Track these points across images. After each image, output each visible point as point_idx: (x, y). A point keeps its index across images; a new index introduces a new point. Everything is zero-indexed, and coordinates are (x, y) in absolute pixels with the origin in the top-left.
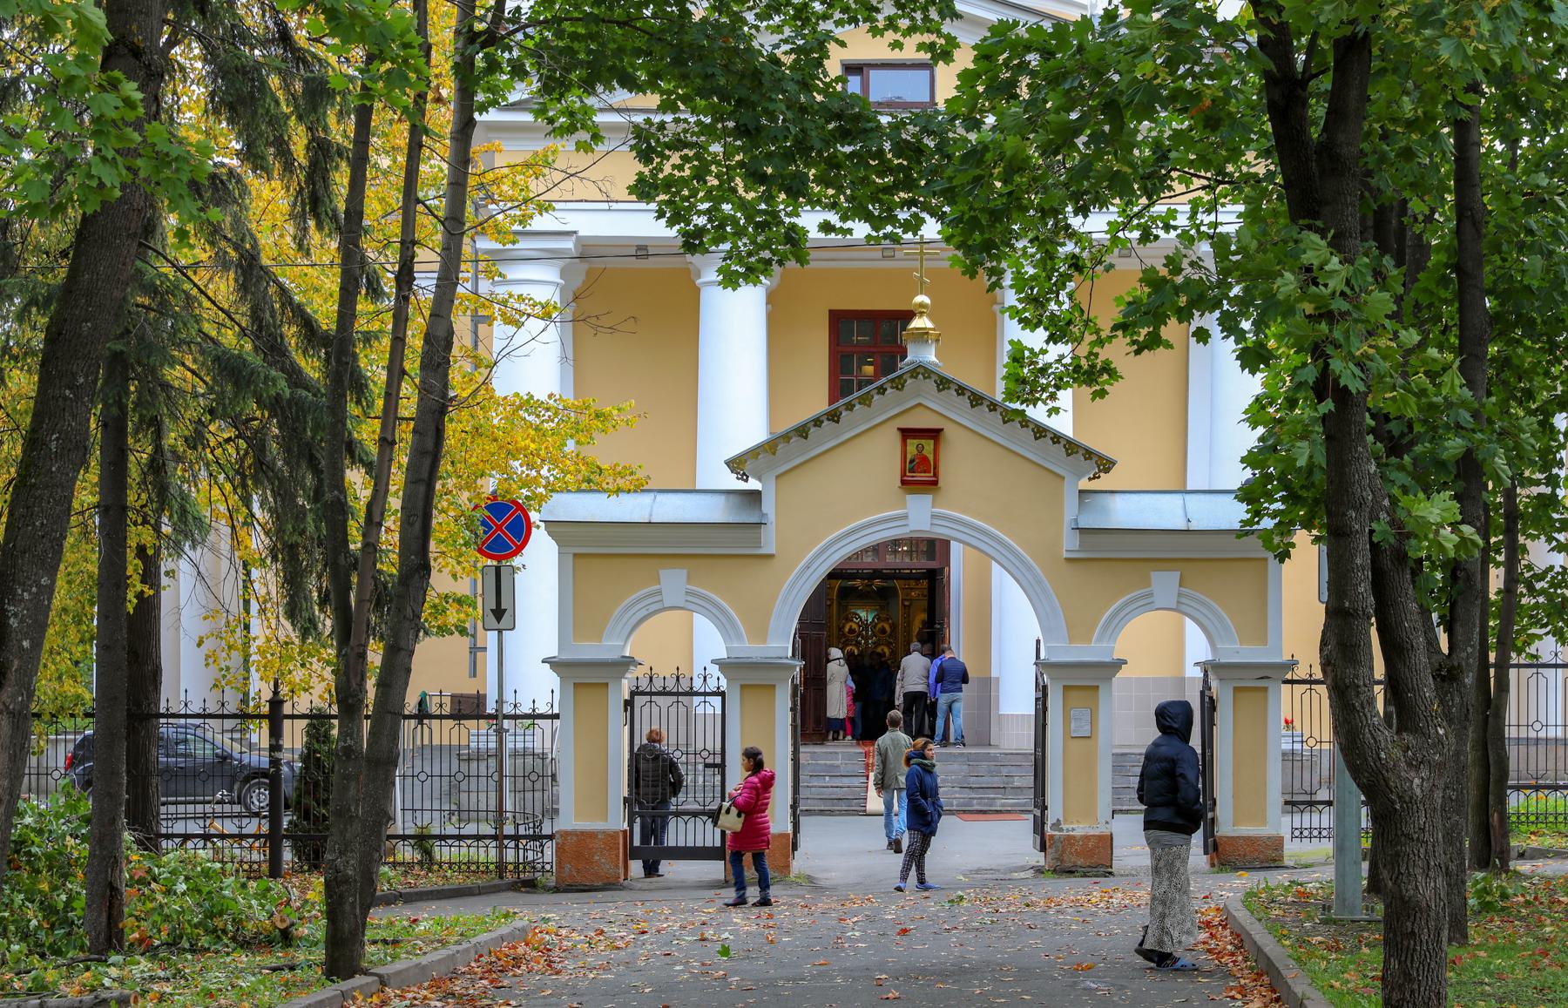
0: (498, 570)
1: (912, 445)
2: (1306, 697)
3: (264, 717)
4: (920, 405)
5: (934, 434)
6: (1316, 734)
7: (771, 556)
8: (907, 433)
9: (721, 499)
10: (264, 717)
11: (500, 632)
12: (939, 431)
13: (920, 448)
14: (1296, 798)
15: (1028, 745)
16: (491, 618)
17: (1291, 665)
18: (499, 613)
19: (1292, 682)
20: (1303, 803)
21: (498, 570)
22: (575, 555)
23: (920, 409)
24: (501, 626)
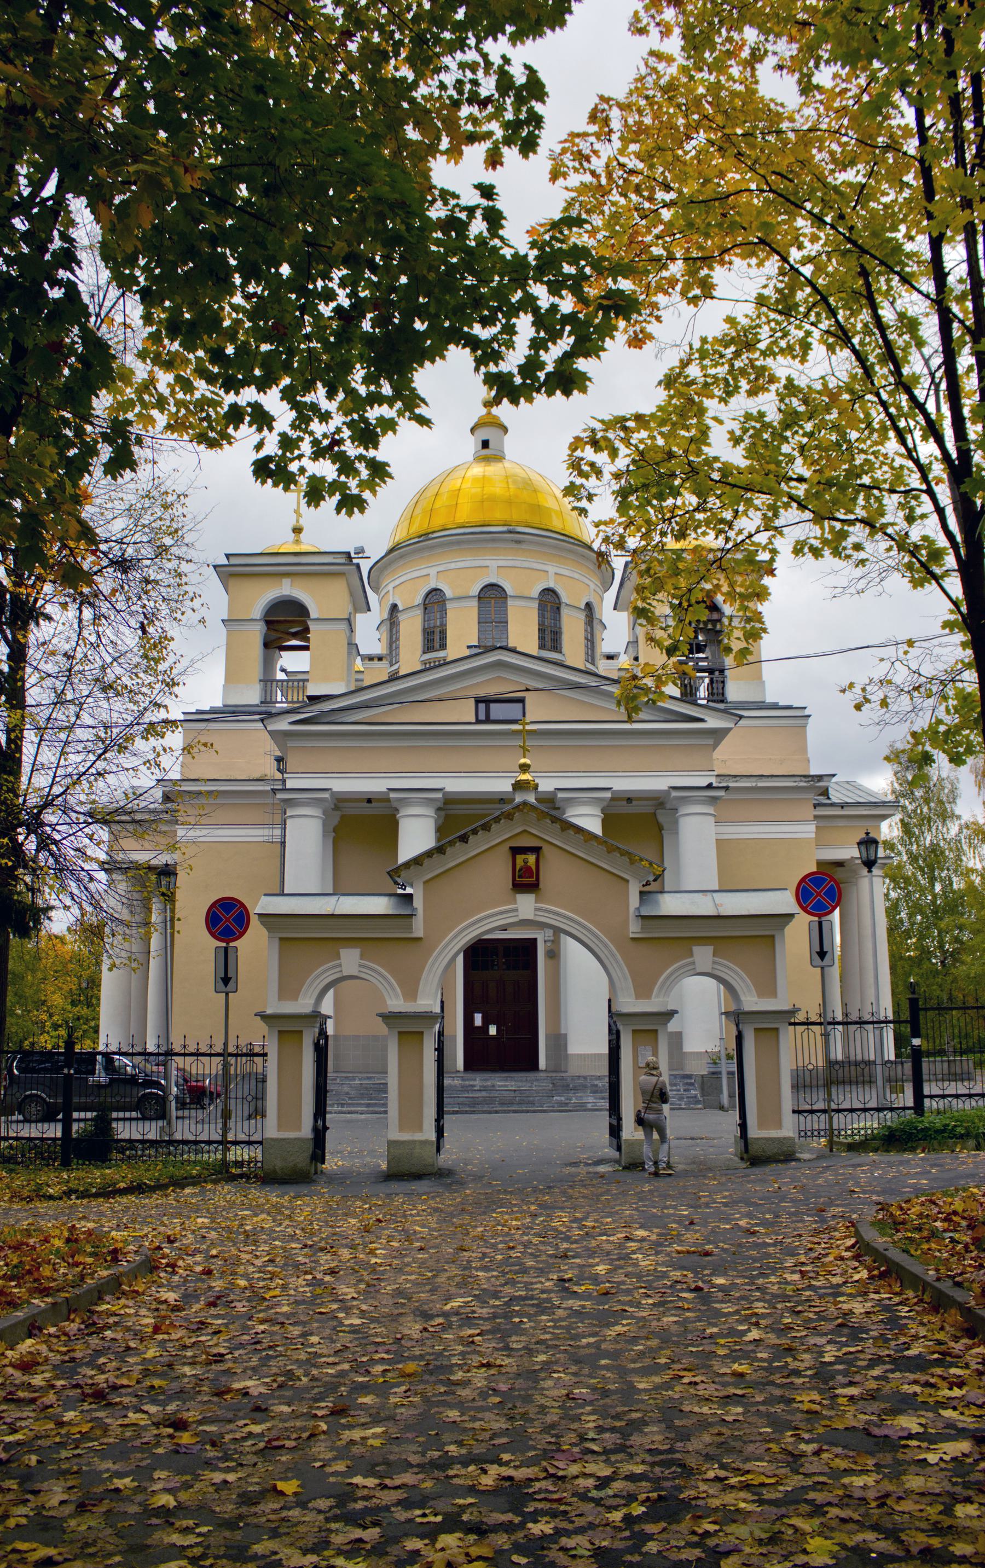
1: (520, 859)
5: (536, 850)
7: (419, 939)
8: (516, 851)
16: (221, 984)
18: (226, 980)
19: (795, 1024)
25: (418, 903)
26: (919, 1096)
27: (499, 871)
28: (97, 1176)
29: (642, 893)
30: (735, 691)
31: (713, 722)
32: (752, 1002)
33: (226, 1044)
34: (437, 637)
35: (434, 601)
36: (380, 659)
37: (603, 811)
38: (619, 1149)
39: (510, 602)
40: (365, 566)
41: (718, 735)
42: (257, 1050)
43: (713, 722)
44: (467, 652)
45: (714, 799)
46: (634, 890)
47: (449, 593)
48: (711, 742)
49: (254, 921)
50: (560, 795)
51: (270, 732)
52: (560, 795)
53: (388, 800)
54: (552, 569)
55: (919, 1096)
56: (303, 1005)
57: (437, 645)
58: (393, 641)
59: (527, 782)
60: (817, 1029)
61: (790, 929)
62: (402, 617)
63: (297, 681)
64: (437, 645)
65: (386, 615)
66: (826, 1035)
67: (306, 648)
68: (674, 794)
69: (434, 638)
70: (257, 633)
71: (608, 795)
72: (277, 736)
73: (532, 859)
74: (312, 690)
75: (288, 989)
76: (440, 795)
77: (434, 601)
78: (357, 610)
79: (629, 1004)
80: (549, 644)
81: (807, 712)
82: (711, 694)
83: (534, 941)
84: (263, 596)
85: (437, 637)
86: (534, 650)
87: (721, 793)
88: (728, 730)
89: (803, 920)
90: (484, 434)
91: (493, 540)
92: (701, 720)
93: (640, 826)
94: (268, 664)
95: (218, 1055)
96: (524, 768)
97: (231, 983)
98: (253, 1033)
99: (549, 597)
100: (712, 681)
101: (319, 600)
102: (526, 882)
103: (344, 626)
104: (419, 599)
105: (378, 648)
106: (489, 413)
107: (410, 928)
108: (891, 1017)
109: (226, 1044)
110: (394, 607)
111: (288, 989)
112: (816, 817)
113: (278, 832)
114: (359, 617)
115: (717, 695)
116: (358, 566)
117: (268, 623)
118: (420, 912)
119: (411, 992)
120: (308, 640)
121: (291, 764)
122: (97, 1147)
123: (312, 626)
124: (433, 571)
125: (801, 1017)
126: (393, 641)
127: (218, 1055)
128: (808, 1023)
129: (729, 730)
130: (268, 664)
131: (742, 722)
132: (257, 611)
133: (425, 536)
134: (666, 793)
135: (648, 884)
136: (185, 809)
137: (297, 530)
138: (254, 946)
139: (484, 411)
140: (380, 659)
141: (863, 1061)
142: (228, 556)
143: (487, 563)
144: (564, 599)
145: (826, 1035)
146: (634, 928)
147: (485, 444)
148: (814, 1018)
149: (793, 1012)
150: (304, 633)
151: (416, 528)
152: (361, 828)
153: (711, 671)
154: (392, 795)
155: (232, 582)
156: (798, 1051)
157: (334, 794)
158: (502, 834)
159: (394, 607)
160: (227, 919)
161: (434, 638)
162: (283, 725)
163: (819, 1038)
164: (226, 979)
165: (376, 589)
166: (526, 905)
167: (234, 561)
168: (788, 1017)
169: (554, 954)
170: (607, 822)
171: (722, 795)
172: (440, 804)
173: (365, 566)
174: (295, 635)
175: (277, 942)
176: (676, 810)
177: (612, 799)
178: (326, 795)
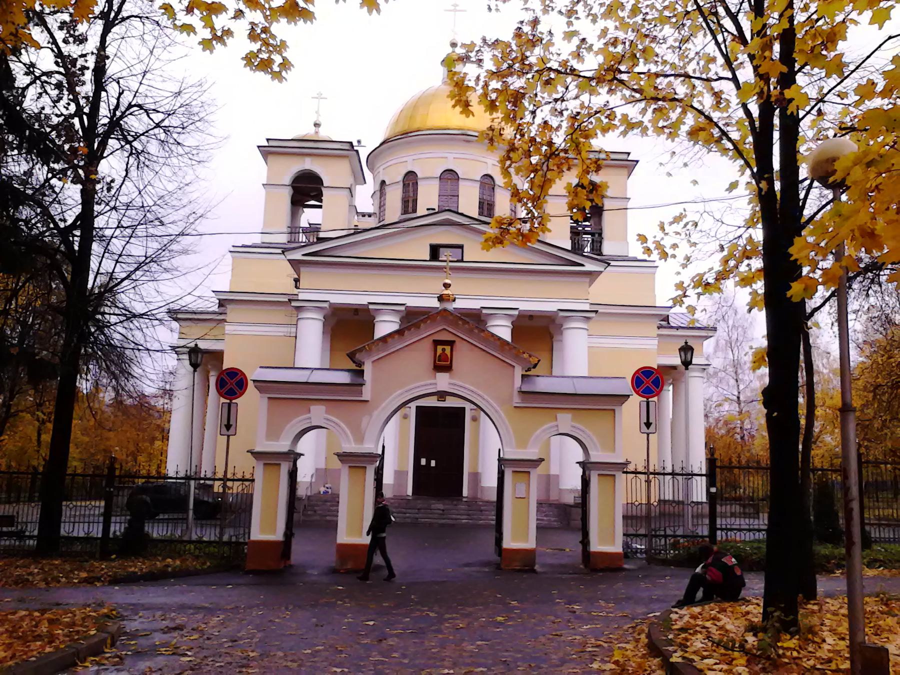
0: (229, 405)
1: (440, 348)
2: (634, 480)
3: (719, 529)
4: (444, 329)
5: (451, 343)
6: (639, 499)
7: (367, 401)
8: (436, 343)
9: (347, 373)
10: (719, 529)
11: (228, 436)
12: (454, 342)
13: (444, 350)
14: (742, 527)
15: (494, 498)
16: (224, 429)
17: (627, 463)
18: (228, 426)
19: (627, 473)
20: (875, 524)
21: (229, 405)
22: (514, 472)
23: (445, 332)
24: (230, 433)
25: (368, 376)
26: (713, 528)
27: (423, 356)
28: (138, 566)
29: (523, 376)
30: (608, 248)
31: (590, 266)
32: (597, 456)
33: (226, 472)
34: (411, 205)
35: (410, 180)
36: (370, 216)
37: (512, 323)
38: (500, 555)
39: (461, 183)
40: (364, 154)
41: (592, 276)
42: (248, 476)
43: (590, 266)
44: (427, 213)
45: (588, 318)
46: (519, 372)
47: (419, 175)
48: (588, 280)
49: (250, 384)
50: (484, 311)
51: (289, 260)
52: (484, 311)
53: (368, 310)
55: (713, 528)
56: (283, 445)
57: (410, 210)
58: (382, 206)
59: (448, 295)
60: (643, 477)
61: (627, 405)
62: (388, 190)
63: (314, 229)
64: (410, 210)
65: (378, 187)
66: (648, 482)
67: (320, 207)
68: (562, 314)
69: (409, 204)
70: (286, 195)
71: (516, 313)
72: (295, 264)
74: (322, 235)
75: (273, 432)
76: (403, 308)
77: (410, 180)
78: (357, 182)
79: (509, 454)
80: (485, 213)
82: (592, 249)
84: (291, 168)
85: (411, 205)
86: (476, 216)
87: (593, 315)
88: (601, 272)
89: (635, 400)
91: (452, 140)
92: (583, 265)
93: (537, 333)
94: (294, 216)
95: (220, 479)
96: (447, 286)
97: (232, 429)
98: (242, 464)
99: (488, 181)
100: (593, 240)
101: (331, 174)
102: (443, 365)
103: (347, 192)
104: (400, 178)
105: (370, 209)
107: (360, 393)
108: (704, 472)
109: (226, 472)
110: (383, 182)
111: (273, 432)
112: (659, 335)
113: (294, 330)
114: (358, 187)
115: (597, 248)
116: (357, 151)
117: (293, 187)
119: (360, 439)
120: (321, 201)
121: (302, 284)
122: (134, 543)
123: (325, 191)
125: (631, 468)
126: (382, 206)
127: (220, 479)
128: (636, 472)
129: (601, 272)
130: (294, 216)
131: (609, 268)
132: (287, 179)
133: (405, 134)
134: (555, 313)
135: (529, 370)
136: (232, 313)
137: (317, 125)
138: (251, 403)
140: (370, 216)
141: (674, 501)
142: (268, 140)
143: (446, 155)
145: (648, 482)
146: (517, 400)
148: (641, 469)
149: (627, 463)
150: (319, 197)
151: (400, 129)
152: (349, 328)
153: (593, 234)
154: (371, 307)
156: (628, 492)
157: (331, 305)
158: (429, 331)
159: (383, 182)
160: (231, 384)
161: (409, 204)
162: (297, 255)
163: (644, 484)
164: (228, 426)
165: (371, 169)
166: (443, 381)
168: (622, 467)
169: (475, 419)
170: (516, 330)
171: (589, 315)
172: (404, 314)
173: (364, 154)
174: (313, 198)
175: (266, 400)
176: (562, 326)
177: (519, 316)
178: (326, 305)
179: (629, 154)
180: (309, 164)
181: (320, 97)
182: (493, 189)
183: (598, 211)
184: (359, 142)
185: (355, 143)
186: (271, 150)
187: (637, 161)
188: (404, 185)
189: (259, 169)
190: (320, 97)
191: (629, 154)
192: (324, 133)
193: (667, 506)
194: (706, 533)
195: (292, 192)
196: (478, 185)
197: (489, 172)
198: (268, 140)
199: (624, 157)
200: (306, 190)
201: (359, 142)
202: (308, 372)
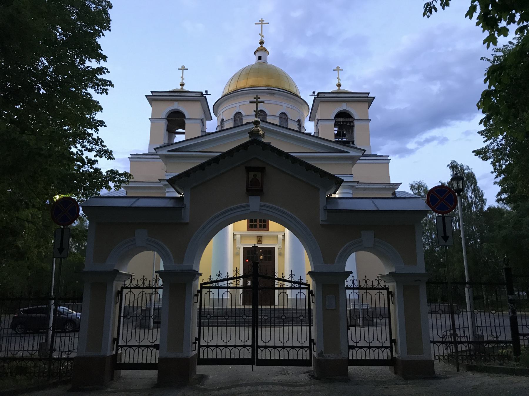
1: (251, 175)
5: (262, 170)
7: (187, 224)
12: (264, 168)
13: (255, 176)
47: (244, 114)
54: (285, 105)
70: (163, 125)
73: (259, 175)
81: (389, 158)
83: (273, 248)
90: (259, 54)
92: (348, 152)
99: (283, 116)
101: (190, 111)
103: (199, 122)
106: (262, 46)
110: (223, 120)
116: (205, 97)
117: (168, 120)
118: (188, 206)
123: (187, 122)
124: (238, 105)
139: (260, 45)
142: (152, 92)
144: (289, 117)
147: (260, 58)
151: (232, 88)
155: (154, 103)
159: (223, 120)
165: (216, 114)
167: (154, 94)
173: (211, 101)
179: (368, 94)
180: (176, 106)
181: (183, 68)
182: (287, 121)
183: (350, 128)
184: (206, 92)
185: (204, 93)
186: (154, 98)
187: (374, 98)
188: (235, 120)
189: (147, 109)
190: (183, 68)
191: (368, 94)
192: (185, 88)
193: (437, 309)
194: (509, 337)
195: (167, 123)
196: (278, 118)
197: (284, 111)
198: (152, 92)
199: (366, 95)
200: (175, 121)
201: (206, 92)
202: (134, 200)
